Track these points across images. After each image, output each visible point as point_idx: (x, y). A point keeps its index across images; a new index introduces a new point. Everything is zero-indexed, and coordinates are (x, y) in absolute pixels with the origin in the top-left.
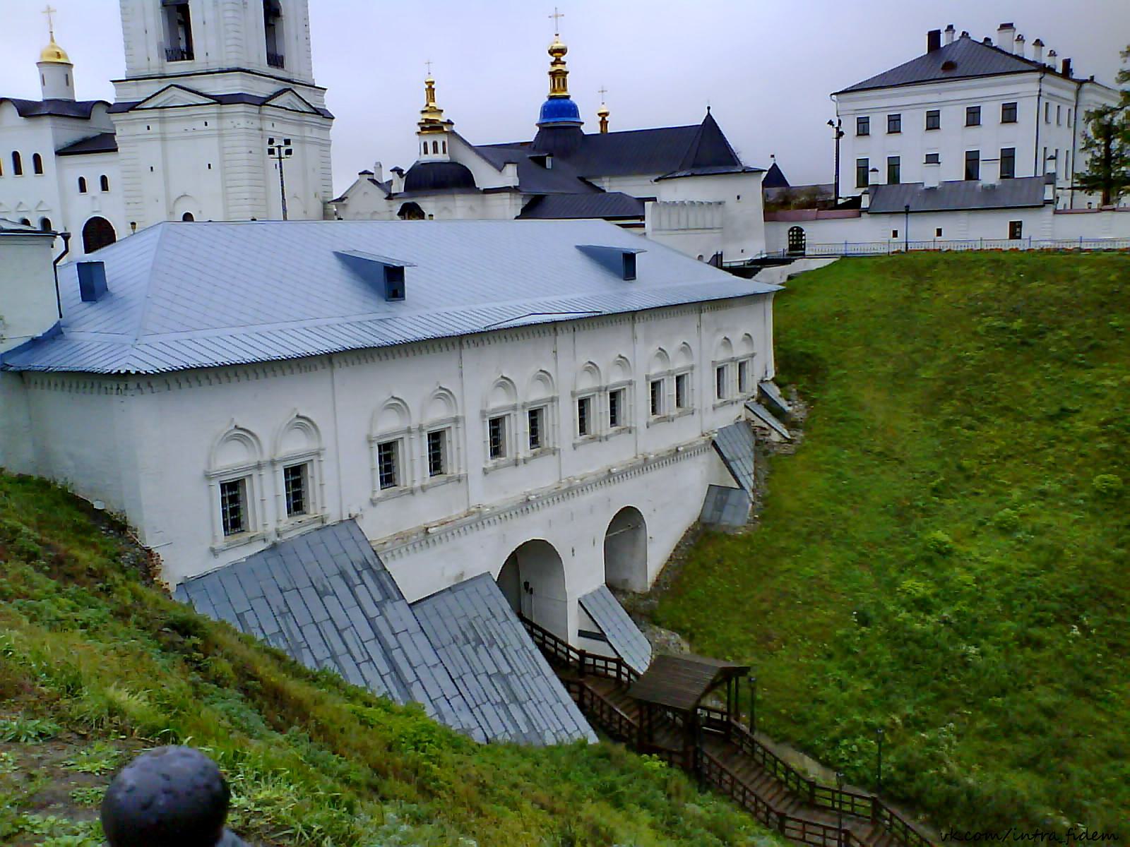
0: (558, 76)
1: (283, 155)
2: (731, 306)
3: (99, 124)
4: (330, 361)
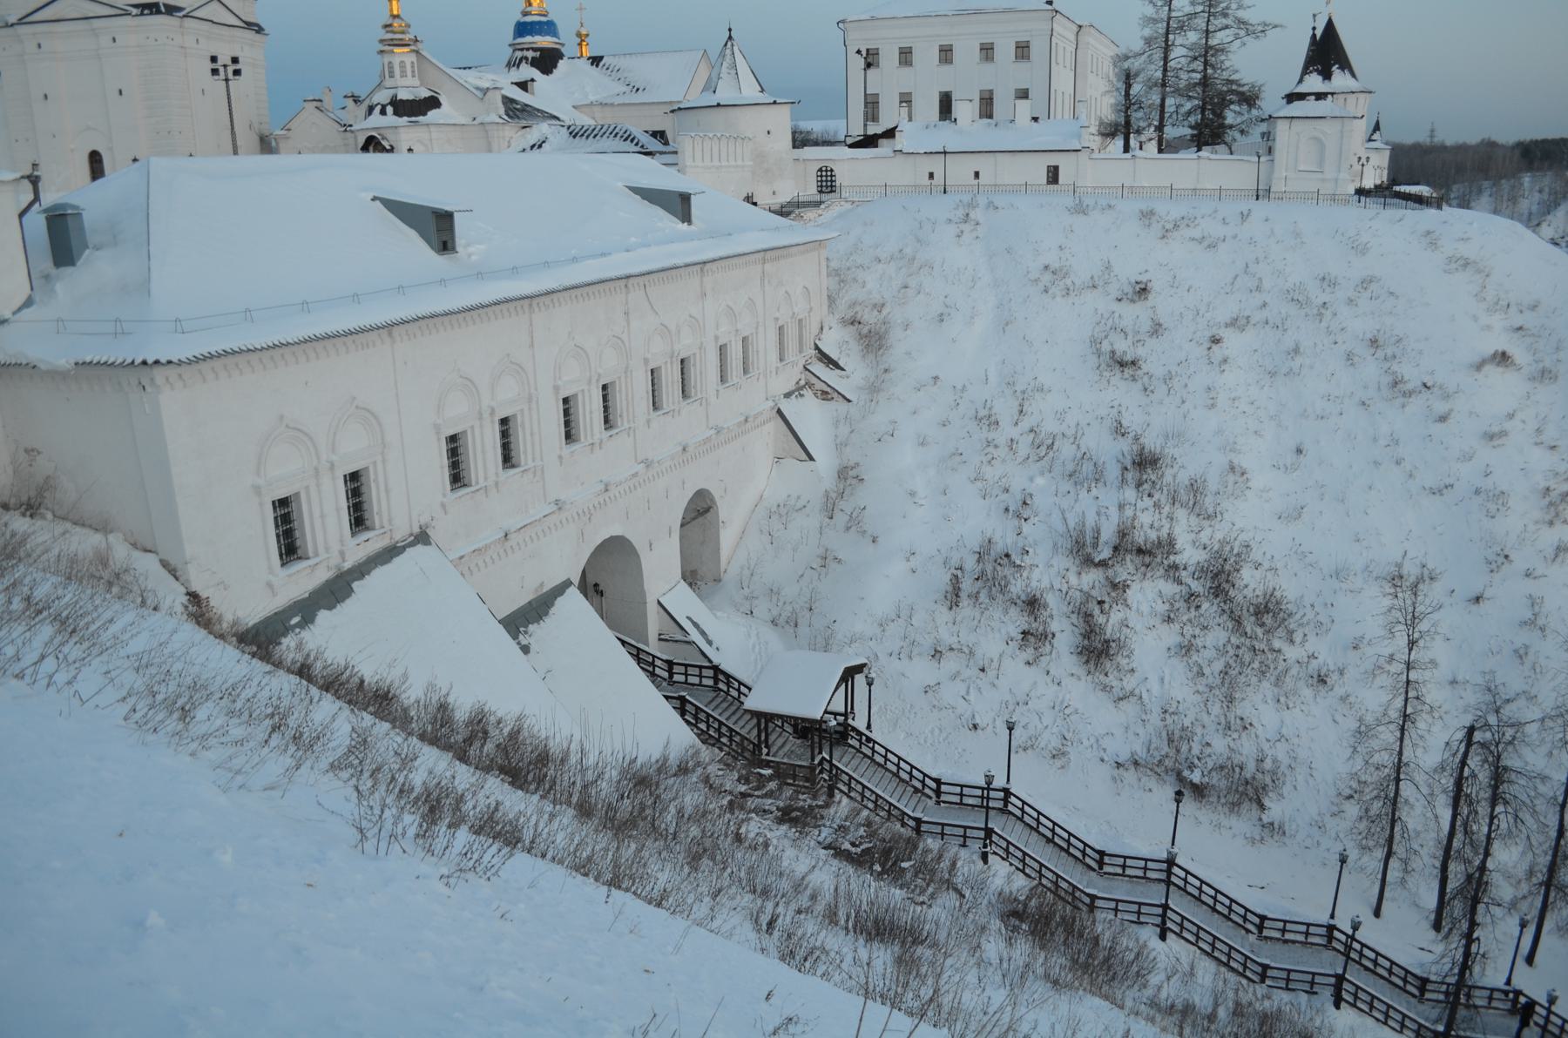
1: (230, 75)
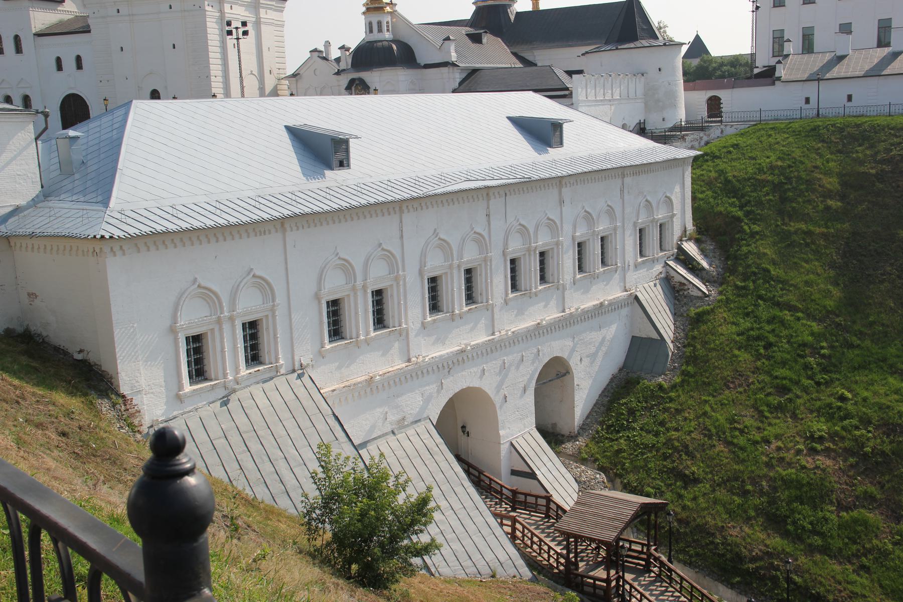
1: (241, 36)
4: (282, 225)
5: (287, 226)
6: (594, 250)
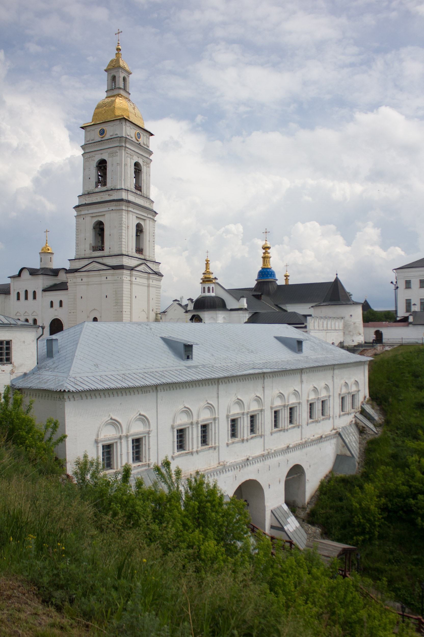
0: (265, 258)
2: (349, 367)
3: (62, 277)
5: (158, 388)
6: (318, 407)
